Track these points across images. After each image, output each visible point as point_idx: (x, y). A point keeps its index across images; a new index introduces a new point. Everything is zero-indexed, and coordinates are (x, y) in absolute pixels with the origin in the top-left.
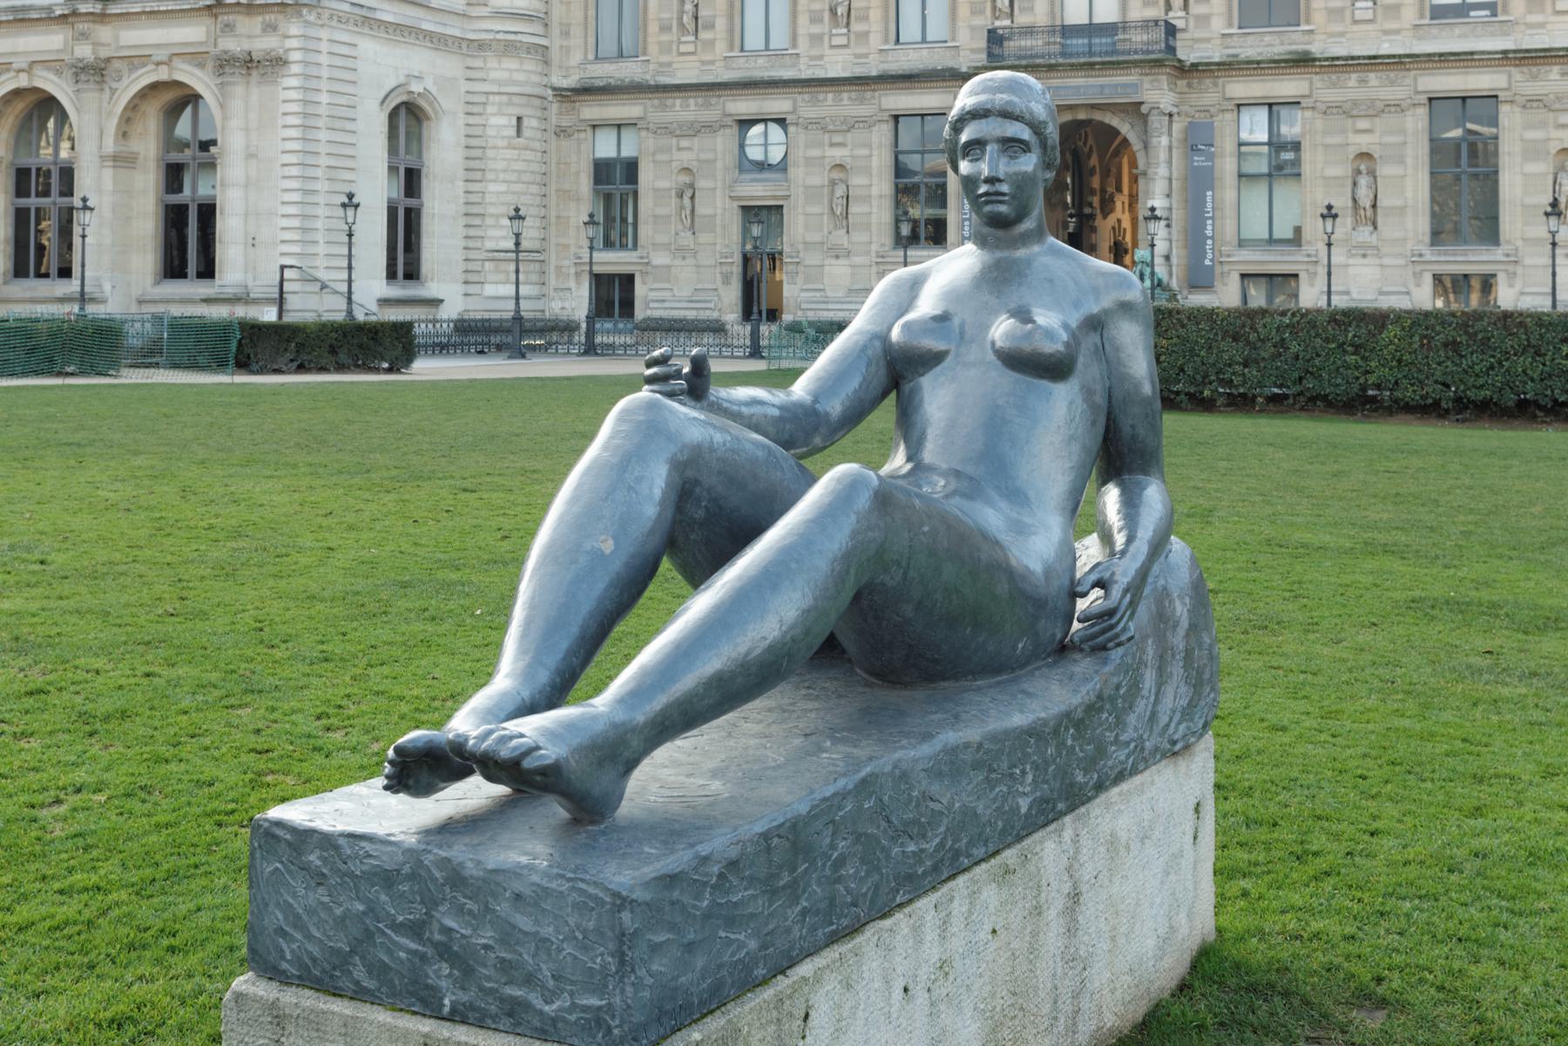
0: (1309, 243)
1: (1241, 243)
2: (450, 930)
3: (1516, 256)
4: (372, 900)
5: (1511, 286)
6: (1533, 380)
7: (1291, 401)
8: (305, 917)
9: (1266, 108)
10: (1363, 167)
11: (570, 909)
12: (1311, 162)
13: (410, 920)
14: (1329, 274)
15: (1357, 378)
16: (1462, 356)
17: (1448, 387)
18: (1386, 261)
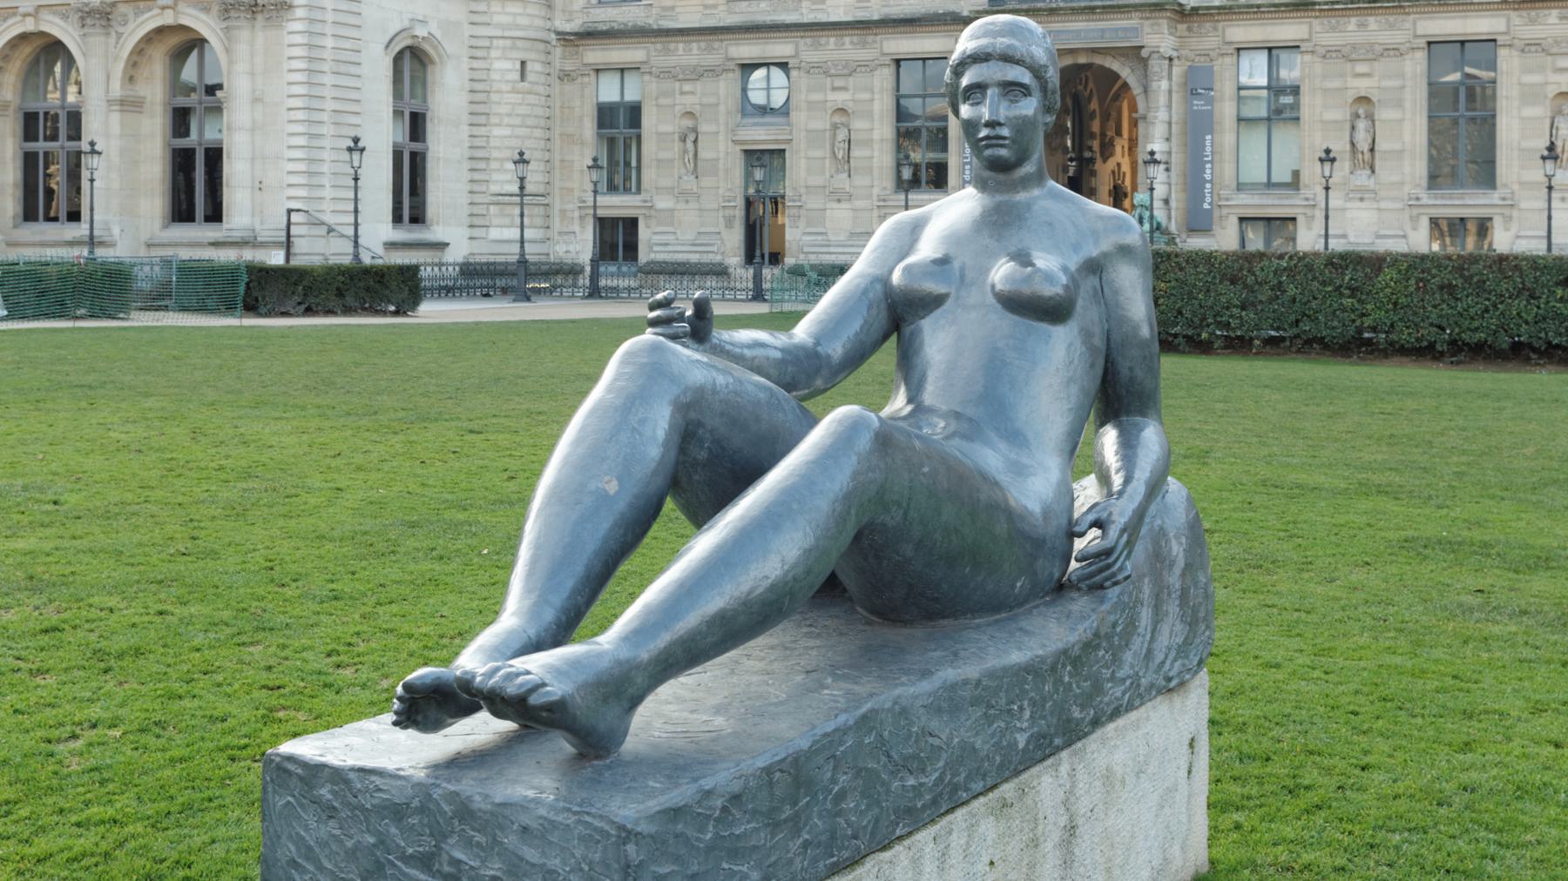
0: (1306, 186)
1: (1240, 187)
2: (459, 862)
3: (1512, 199)
4: (381, 833)
5: (1507, 229)
6: (1527, 323)
7: (1288, 343)
8: (317, 850)
9: (1266, 52)
10: (1361, 111)
11: (576, 842)
12: (1311, 105)
13: (419, 852)
14: (1327, 218)
15: (1354, 321)
16: (1457, 299)
17: (1443, 329)
18: (1383, 205)
